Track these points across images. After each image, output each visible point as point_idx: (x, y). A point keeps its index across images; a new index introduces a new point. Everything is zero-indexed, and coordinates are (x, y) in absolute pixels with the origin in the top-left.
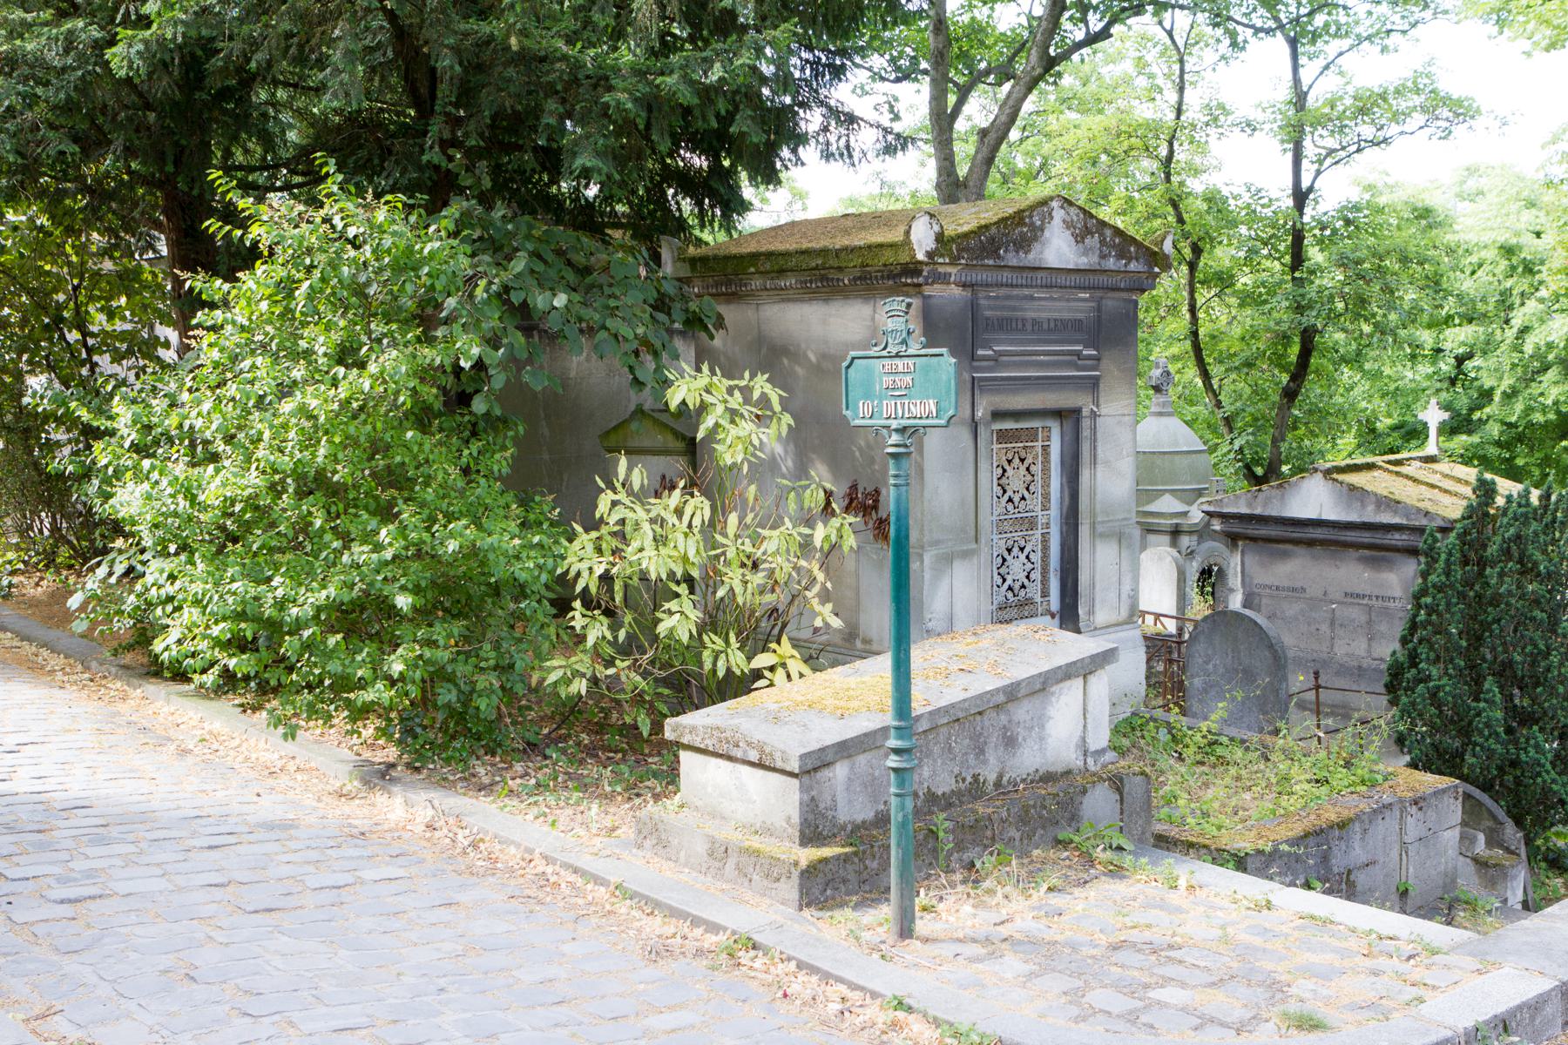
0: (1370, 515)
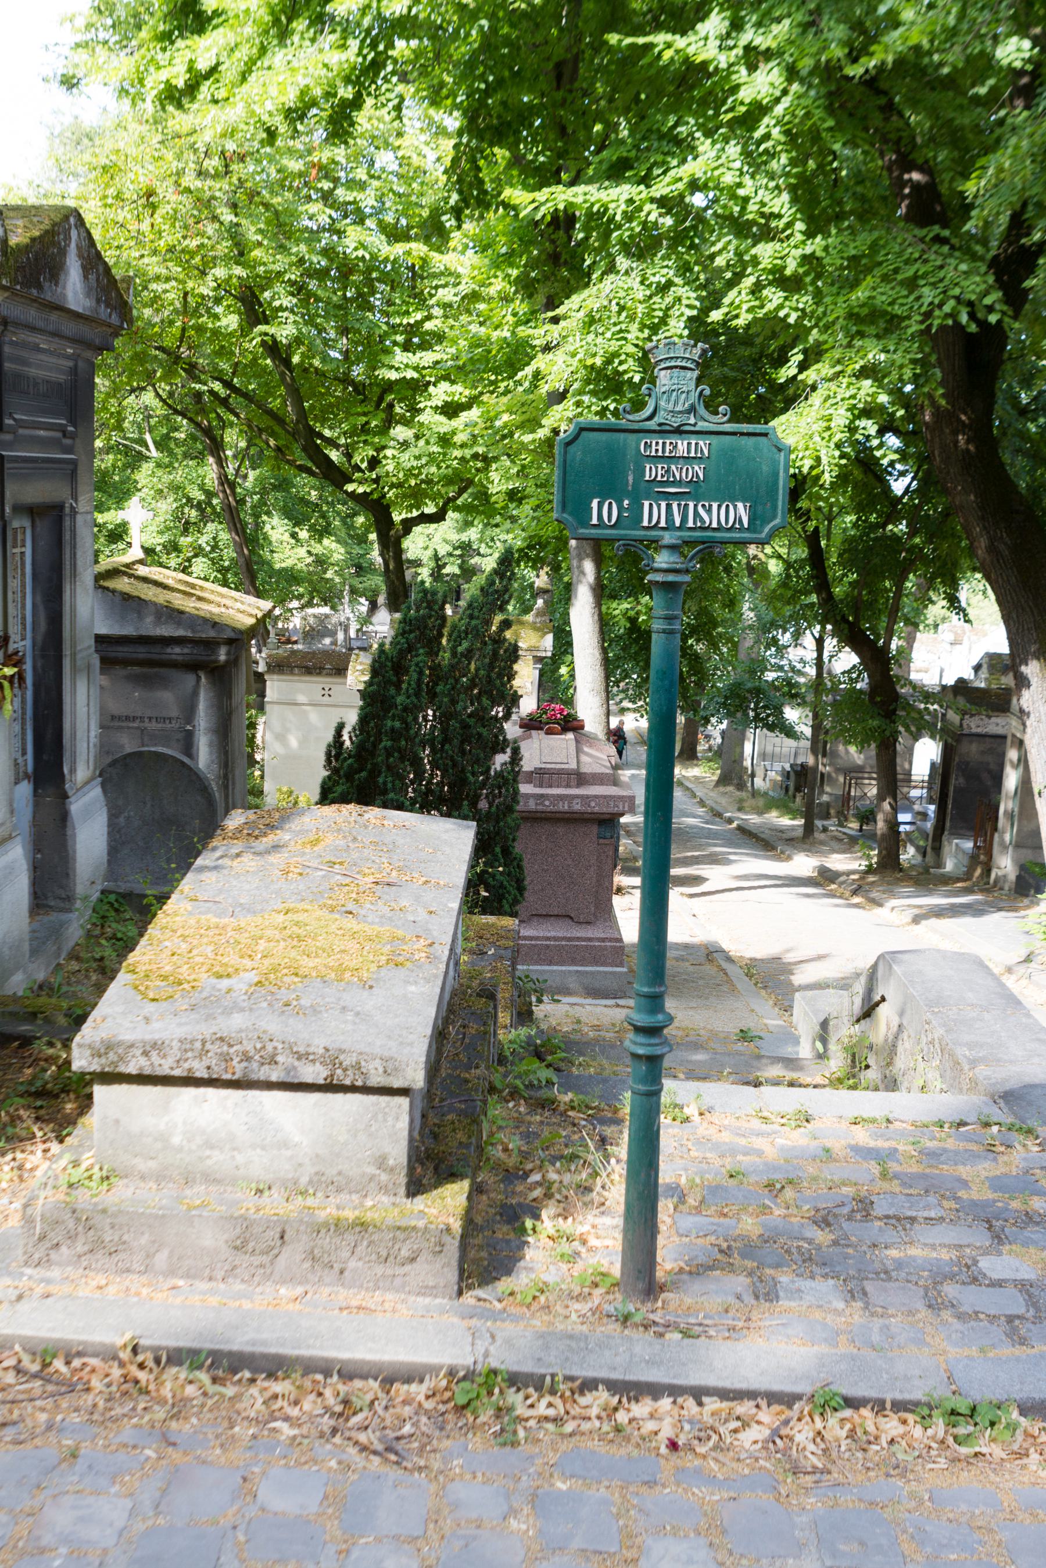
0: (150, 628)
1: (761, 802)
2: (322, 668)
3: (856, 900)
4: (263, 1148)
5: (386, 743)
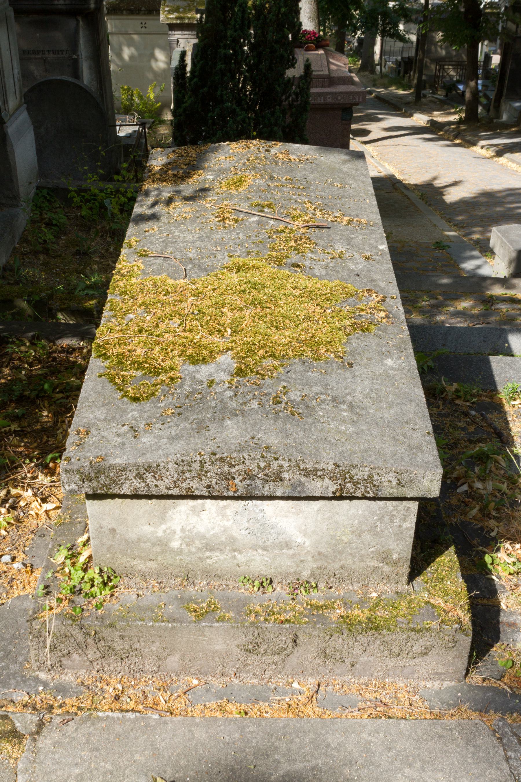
1: (386, 81)
2: (140, 10)
3: (458, 141)
4: (265, 549)
5: (220, 66)
